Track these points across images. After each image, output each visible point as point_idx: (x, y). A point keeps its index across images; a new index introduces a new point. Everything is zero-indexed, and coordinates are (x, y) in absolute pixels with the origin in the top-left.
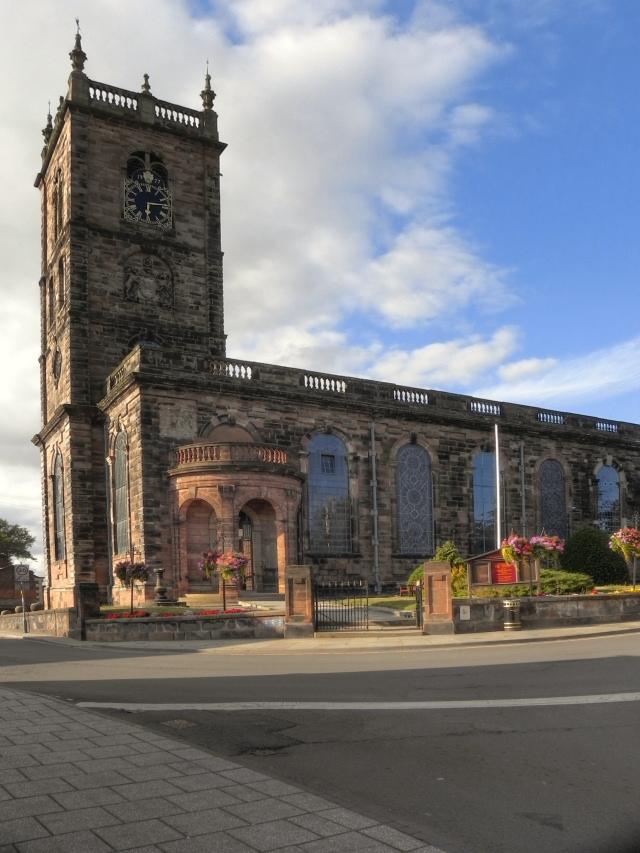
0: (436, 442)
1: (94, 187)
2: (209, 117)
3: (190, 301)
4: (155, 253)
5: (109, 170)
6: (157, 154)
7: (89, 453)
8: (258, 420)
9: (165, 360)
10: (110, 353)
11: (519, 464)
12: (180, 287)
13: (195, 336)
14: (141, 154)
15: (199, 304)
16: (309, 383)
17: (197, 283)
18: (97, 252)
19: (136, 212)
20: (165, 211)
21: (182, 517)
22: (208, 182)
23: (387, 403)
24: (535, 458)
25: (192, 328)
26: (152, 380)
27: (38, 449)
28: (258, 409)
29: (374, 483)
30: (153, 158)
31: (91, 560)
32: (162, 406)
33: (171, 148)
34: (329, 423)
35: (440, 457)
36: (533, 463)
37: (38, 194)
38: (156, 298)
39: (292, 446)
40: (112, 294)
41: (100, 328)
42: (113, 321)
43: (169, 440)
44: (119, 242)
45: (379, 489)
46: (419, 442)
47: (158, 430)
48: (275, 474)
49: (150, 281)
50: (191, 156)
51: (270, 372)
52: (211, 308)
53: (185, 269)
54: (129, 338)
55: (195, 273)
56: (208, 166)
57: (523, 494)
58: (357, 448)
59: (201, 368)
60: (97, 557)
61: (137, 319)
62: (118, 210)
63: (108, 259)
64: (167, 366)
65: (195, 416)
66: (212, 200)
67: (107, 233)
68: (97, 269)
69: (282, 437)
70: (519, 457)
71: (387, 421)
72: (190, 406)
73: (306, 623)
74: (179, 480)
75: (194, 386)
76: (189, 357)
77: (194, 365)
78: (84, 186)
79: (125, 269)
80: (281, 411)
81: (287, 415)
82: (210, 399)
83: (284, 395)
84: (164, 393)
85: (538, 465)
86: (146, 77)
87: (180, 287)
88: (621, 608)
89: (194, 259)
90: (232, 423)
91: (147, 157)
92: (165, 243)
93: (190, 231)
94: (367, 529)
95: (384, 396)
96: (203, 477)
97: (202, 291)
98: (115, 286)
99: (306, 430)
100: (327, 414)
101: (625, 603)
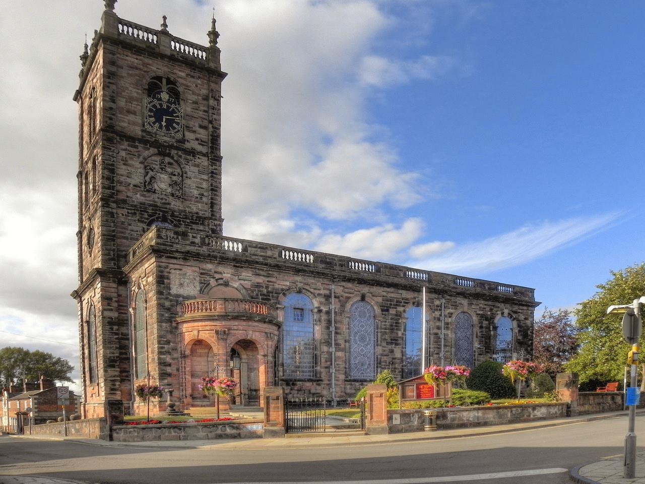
0: (380, 299)
1: (122, 103)
2: (213, 52)
3: (196, 193)
4: (169, 155)
5: (134, 90)
6: (172, 79)
7: (115, 305)
8: (246, 282)
9: (175, 236)
10: (132, 231)
11: (441, 315)
12: (188, 182)
13: (199, 220)
14: (159, 78)
15: (203, 195)
16: (285, 255)
17: (201, 179)
18: (123, 154)
19: (154, 123)
20: (178, 124)
21: (188, 352)
22: (212, 102)
23: (344, 271)
25: (197, 213)
26: (165, 251)
27: (76, 301)
29: (333, 329)
30: (169, 81)
31: (118, 383)
33: (183, 74)
35: (382, 310)
36: (450, 315)
37: (76, 106)
38: (169, 190)
40: (135, 186)
41: (125, 211)
42: (135, 206)
43: (178, 296)
44: (141, 147)
45: (336, 333)
48: (259, 321)
49: (165, 177)
50: (199, 82)
51: (256, 247)
52: (212, 199)
53: (192, 168)
54: (147, 219)
57: (442, 336)
58: (321, 303)
59: (203, 243)
60: (122, 381)
62: (140, 122)
63: (131, 159)
64: (177, 241)
65: (198, 279)
66: (214, 116)
67: (131, 139)
68: (124, 167)
69: (264, 295)
70: (440, 310)
72: (195, 271)
73: (280, 428)
74: (185, 325)
75: (197, 256)
76: (195, 235)
77: (197, 240)
78: (114, 101)
79: (145, 167)
80: (264, 276)
81: (269, 279)
82: (209, 266)
83: (266, 264)
85: (454, 317)
86: (165, 18)
87: (188, 182)
88: (509, 415)
89: (200, 161)
90: (226, 284)
91: (164, 81)
92: (177, 148)
93: (197, 139)
94: (326, 361)
95: (341, 265)
96: (203, 323)
97: (205, 185)
98: (137, 178)
99: (282, 290)
100: (298, 278)
101: (511, 411)
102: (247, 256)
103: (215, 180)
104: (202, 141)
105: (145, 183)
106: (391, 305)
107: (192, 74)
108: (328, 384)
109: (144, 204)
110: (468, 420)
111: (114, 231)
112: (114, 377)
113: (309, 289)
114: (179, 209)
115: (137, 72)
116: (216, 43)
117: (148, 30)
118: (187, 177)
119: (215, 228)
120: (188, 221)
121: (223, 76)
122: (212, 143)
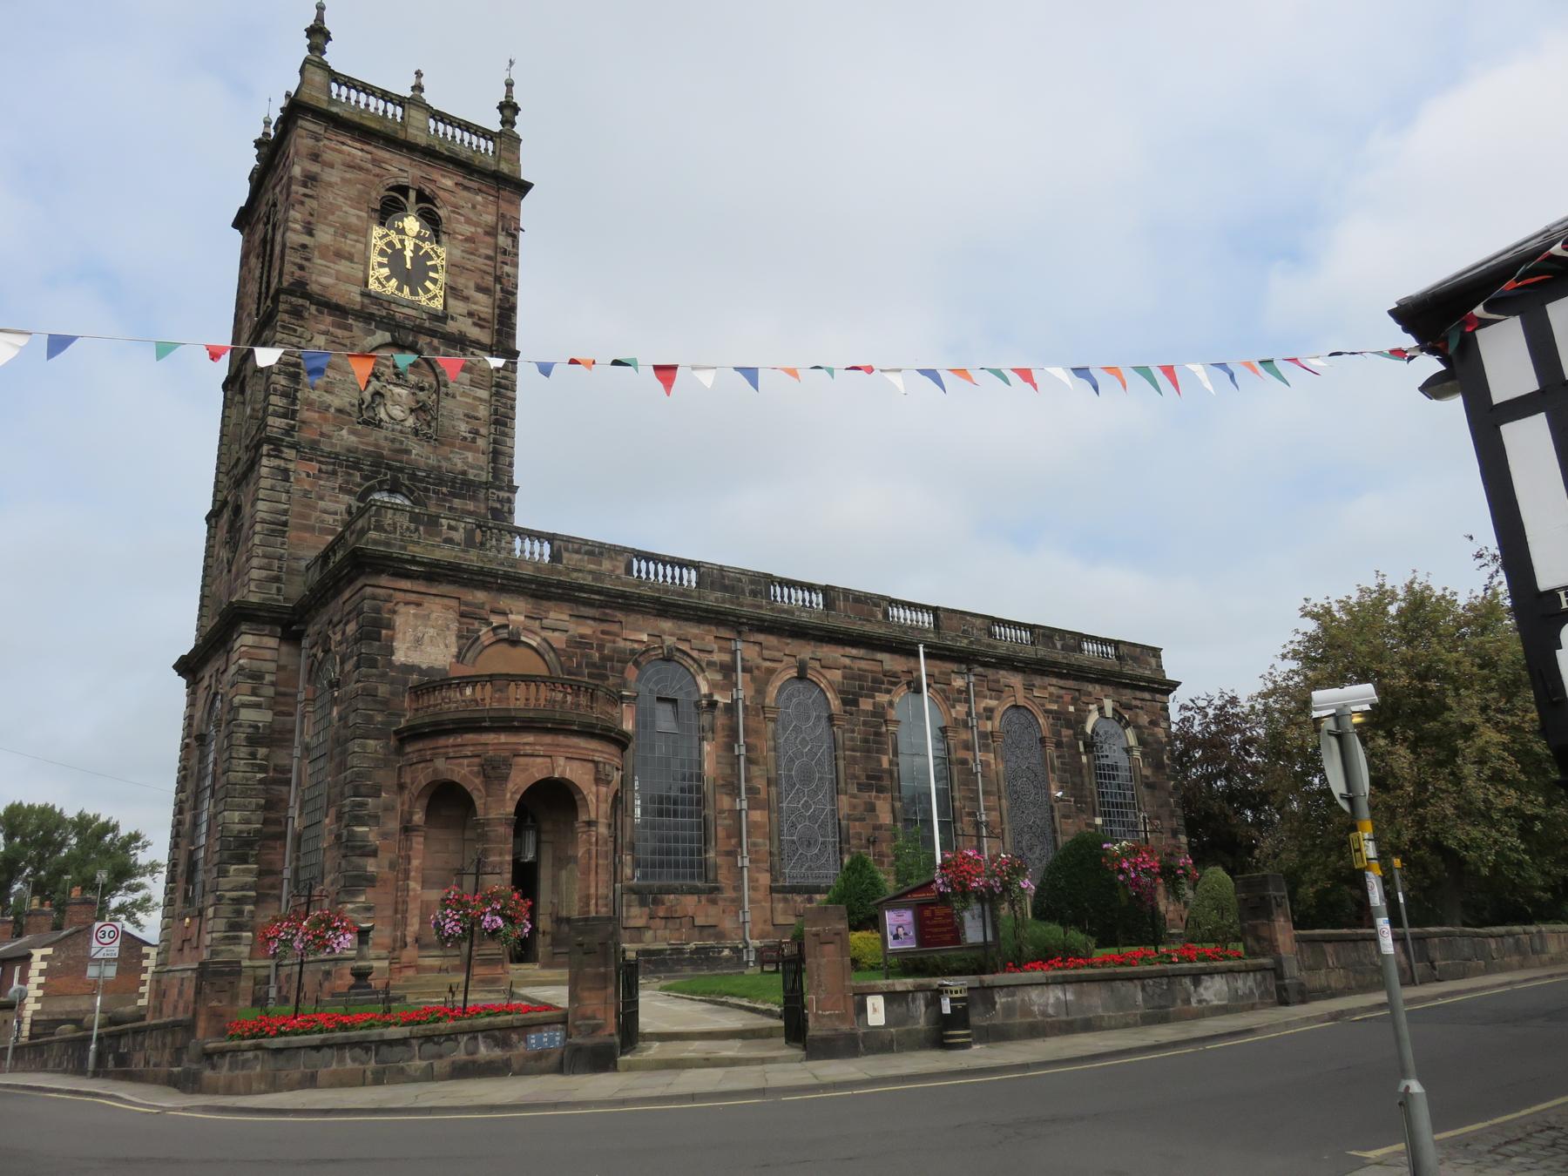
0: (836, 675)
2: (507, 139)
3: (463, 428)
4: (413, 348)
6: (427, 192)
7: (270, 691)
8: (557, 634)
9: (413, 526)
10: (325, 512)
11: (969, 714)
13: (464, 486)
14: (403, 190)
15: (477, 433)
16: (639, 571)
17: (475, 398)
19: (388, 279)
23: (760, 607)
24: (993, 703)
25: (464, 473)
28: (558, 615)
30: (422, 197)
32: (401, 608)
33: (448, 183)
34: (670, 641)
35: (845, 702)
37: (237, 237)
38: (410, 421)
39: (612, 680)
40: (339, 411)
42: (337, 456)
44: (358, 326)
45: (749, 761)
46: (811, 674)
47: (391, 651)
50: (479, 198)
51: (578, 552)
54: (360, 485)
55: (473, 384)
56: (503, 216)
59: (469, 542)
61: (378, 461)
64: (415, 537)
65: (454, 626)
66: (507, 269)
67: (339, 311)
69: (594, 665)
70: (967, 701)
71: (761, 637)
72: (448, 608)
76: (453, 523)
77: (458, 536)
80: (594, 619)
81: (605, 626)
82: (481, 596)
83: (599, 592)
84: (406, 584)
85: (997, 715)
86: (419, 74)
87: (447, 403)
90: (514, 641)
91: (412, 195)
92: (432, 333)
93: (470, 314)
94: (729, 837)
95: (754, 594)
97: (483, 412)
99: (633, 652)
100: (667, 625)
102: (560, 573)
103: (504, 401)
104: (480, 318)
105: (360, 405)
106: (861, 688)
107: (466, 182)
108: (733, 900)
109: (355, 450)
110: (1044, 1014)
111: (285, 512)
112: (242, 889)
113: (689, 651)
114: (427, 464)
115: (362, 176)
116: (513, 124)
117: (386, 96)
118: (447, 394)
119: (498, 506)
120: (444, 490)
121: (524, 187)
122: (500, 323)
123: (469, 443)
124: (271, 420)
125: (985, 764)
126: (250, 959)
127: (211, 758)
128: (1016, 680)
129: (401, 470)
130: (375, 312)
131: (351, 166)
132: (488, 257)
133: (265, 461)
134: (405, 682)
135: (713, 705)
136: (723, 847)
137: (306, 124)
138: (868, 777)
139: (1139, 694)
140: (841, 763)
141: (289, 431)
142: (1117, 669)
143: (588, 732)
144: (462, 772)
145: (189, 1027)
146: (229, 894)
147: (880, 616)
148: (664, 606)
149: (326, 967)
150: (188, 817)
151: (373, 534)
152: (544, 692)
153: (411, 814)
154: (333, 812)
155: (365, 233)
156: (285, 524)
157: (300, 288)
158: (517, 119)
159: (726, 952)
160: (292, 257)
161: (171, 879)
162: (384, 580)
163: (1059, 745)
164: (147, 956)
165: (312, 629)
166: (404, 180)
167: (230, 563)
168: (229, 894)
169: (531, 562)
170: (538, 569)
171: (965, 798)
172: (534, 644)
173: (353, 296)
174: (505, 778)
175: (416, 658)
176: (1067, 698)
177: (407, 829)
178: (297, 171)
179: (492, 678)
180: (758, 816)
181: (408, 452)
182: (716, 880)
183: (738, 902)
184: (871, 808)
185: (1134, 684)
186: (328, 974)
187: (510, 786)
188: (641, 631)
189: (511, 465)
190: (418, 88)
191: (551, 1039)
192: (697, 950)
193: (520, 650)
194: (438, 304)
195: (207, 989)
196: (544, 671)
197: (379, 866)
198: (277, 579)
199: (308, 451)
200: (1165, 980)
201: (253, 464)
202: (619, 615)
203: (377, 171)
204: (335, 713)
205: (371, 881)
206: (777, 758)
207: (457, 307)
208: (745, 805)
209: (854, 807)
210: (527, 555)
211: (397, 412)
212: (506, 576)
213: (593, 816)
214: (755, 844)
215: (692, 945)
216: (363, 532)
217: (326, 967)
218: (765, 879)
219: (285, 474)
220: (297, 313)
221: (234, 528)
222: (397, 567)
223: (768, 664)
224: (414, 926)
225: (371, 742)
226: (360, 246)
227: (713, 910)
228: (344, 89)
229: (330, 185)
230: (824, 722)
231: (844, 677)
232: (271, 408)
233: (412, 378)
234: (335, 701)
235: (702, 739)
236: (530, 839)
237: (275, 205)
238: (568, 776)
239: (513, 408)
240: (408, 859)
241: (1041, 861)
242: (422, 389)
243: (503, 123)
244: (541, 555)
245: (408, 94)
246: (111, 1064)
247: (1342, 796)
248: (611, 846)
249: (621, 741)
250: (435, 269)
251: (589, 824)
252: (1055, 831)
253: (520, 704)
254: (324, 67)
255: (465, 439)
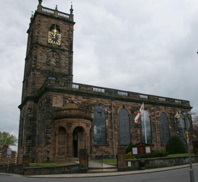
2: (71, 16)
4: (55, 52)
7: (33, 111)
11: (154, 114)
13: (64, 75)
14: (54, 25)
15: (66, 66)
16: (94, 90)
18: (40, 51)
19: (51, 40)
22: (70, 32)
24: (159, 112)
25: (64, 73)
28: (80, 98)
30: (57, 26)
32: (53, 97)
33: (61, 23)
34: (100, 102)
35: (132, 112)
38: (55, 64)
40: (43, 63)
41: (39, 73)
44: (46, 49)
45: (114, 123)
47: (52, 104)
50: (66, 25)
51: (83, 86)
55: (66, 57)
59: (65, 86)
61: (50, 71)
65: (62, 100)
66: (71, 37)
67: (43, 46)
70: (154, 112)
71: (116, 101)
72: (61, 97)
77: (63, 84)
81: (88, 100)
82: (67, 95)
83: (87, 93)
84: (54, 93)
86: (57, 6)
87: (61, 61)
90: (72, 102)
91: (55, 26)
92: (58, 49)
93: (65, 45)
94: (111, 136)
97: (67, 62)
98: (44, 61)
99: (93, 104)
100: (99, 99)
102: (80, 90)
106: (134, 110)
108: (112, 147)
111: (35, 81)
116: (72, 13)
117: (51, 10)
120: (61, 76)
121: (74, 23)
122: (70, 47)
123: (65, 68)
124: (32, 65)
125: (157, 123)
126: (31, 155)
127: (24, 122)
128: (163, 108)
129: (54, 73)
130: (49, 46)
131: (45, 22)
132: (68, 35)
133: (31, 72)
134: (54, 110)
135: (108, 113)
136: (110, 138)
137: (38, 16)
138: (136, 126)
139: (185, 109)
140: (131, 123)
141: (35, 67)
142: (181, 105)
143: (85, 118)
144: (64, 125)
145: (22, 165)
146: (28, 145)
147: (138, 97)
148: (99, 95)
149: (43, 157)
150: (21, 132)
151: (49, 85)
152: (78, 111)
153: (56, 132)
154: (43, 132)
155: (48, 33)
156: (35, 83)
157: (37, 43)
158: (73, 12)
159: (110, 156)
160: (36, 38)
161: (19, 142)
162: (51, 93)
163: (171, 119)
164: (16, 155)
165: (40, 101)
166: (54, 23)
167: (26, 90)
168: (28, 145)
169: (75, 89)
170: (77, 90)
171: (154, 129)
172: (76, 103)
173: (45, 44)
174: (71, 127)
175: (56, 106)
176: (172, 111)
177: (55, 135)
178: (37, 23)
179: (68, 109)
180: (116, 133)
181: (55, 70)
182: (109, 144)
183: (113, 147)
184: (136, 131)
185: (185, 108)
186: (43, 158)
187: (72, 128)
188: (95, 100)
189: (72, 71)
190: (56, 8)
191: (77, 168)
192: (105, 156)
193: (73, 104)
194: (60, 44)
195: (24, 159)
196: (78, 108)
197: (51, 141)
198: (34, 92)
199: (38, 70)
200: (179, 159)
201: (30, 73)
202: (91, 98)
203: (50, 22)
204: (43, 115)
205: (50, 143)
206: (119, 122)
207: (63, 44)
208: (114, 131)
209: (133, 131)
210: (75, 87)
211: (53, 63)
212: (71, 91)
213: (86, 132)
214: (115, 138)
215: (105, 155)
216: (47, 84)
217: (43, 157)
218: (117, 144)
219: (35, 74)
220: (36, 47)
221: (27, 84)
222: (53, 90)
223: (117, 106)
224: (57, 151)
225: (49, 120)
226: (47, 35)
227: (108, 149)
228: (44, 9)
229: (42, 25)
230: (128, 116)
231: (131, 108)
232: (32, 63)
233: (55, 57)
234: (43, 113)
235: (106, 119)
236: (76, 136)
237: (33, 29)
238: (82, 126)
239: (72, 61)
240: (56, 140)
241: (167, 140)
242: (57, 59)
243: (71, 12)
244: (77, 87)
245: (55, 9)
246: (11, 171)
247: (184, 128)
248: (90, 138)
249: (91, 120)
250: (59, 38)
251: (86, 134)
252: (170, 134)
253: (74, 113)
254: (41, 6)
255: (64, 67)
